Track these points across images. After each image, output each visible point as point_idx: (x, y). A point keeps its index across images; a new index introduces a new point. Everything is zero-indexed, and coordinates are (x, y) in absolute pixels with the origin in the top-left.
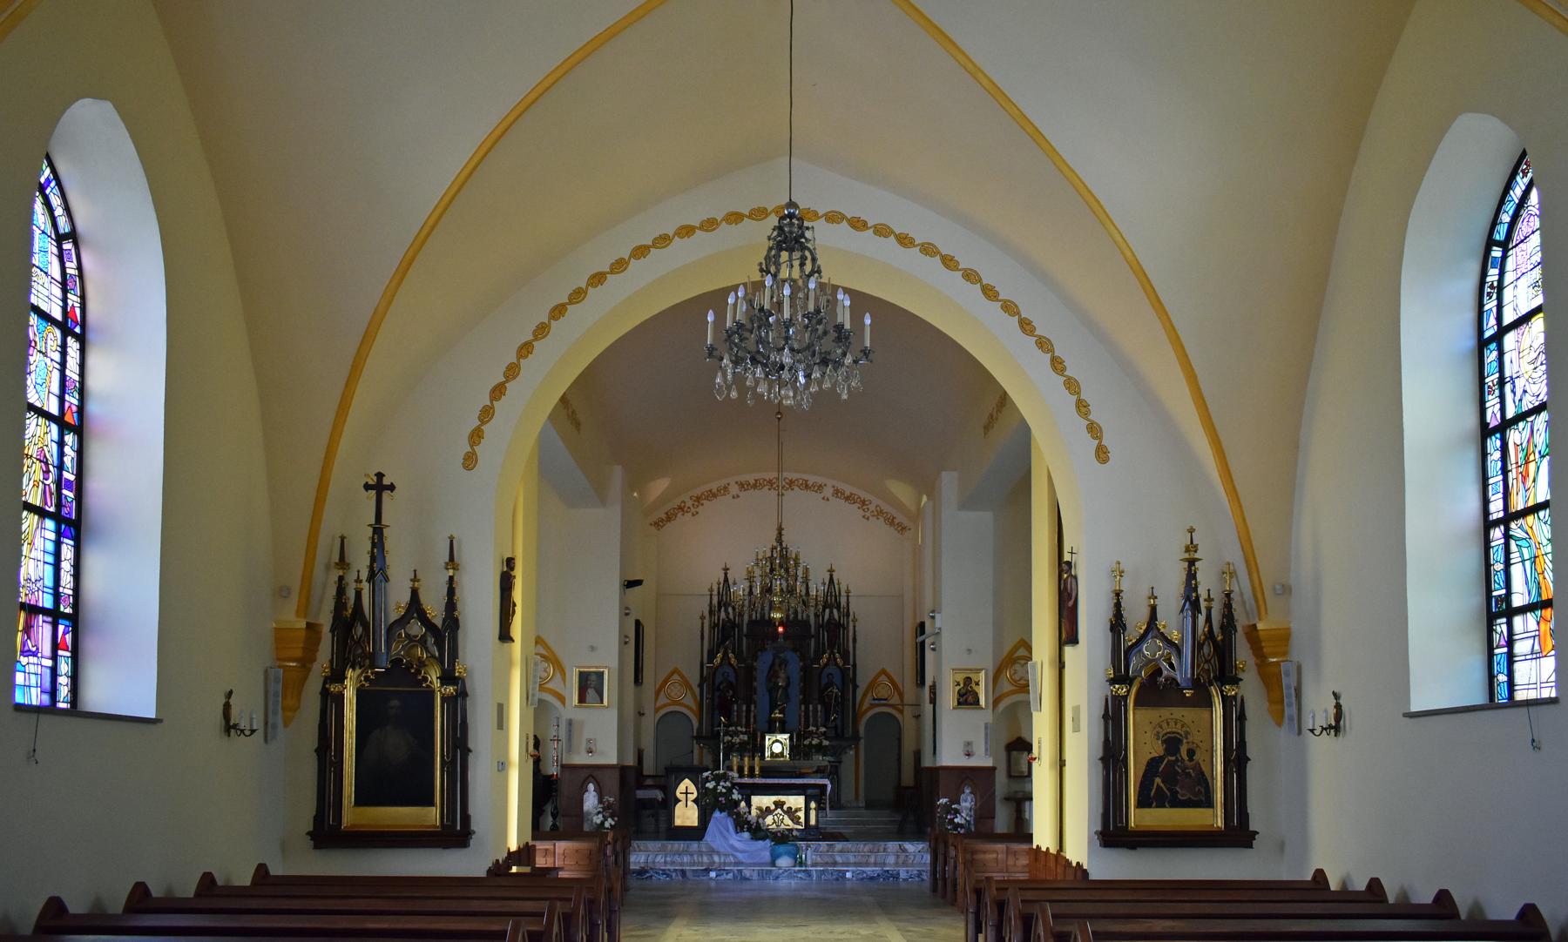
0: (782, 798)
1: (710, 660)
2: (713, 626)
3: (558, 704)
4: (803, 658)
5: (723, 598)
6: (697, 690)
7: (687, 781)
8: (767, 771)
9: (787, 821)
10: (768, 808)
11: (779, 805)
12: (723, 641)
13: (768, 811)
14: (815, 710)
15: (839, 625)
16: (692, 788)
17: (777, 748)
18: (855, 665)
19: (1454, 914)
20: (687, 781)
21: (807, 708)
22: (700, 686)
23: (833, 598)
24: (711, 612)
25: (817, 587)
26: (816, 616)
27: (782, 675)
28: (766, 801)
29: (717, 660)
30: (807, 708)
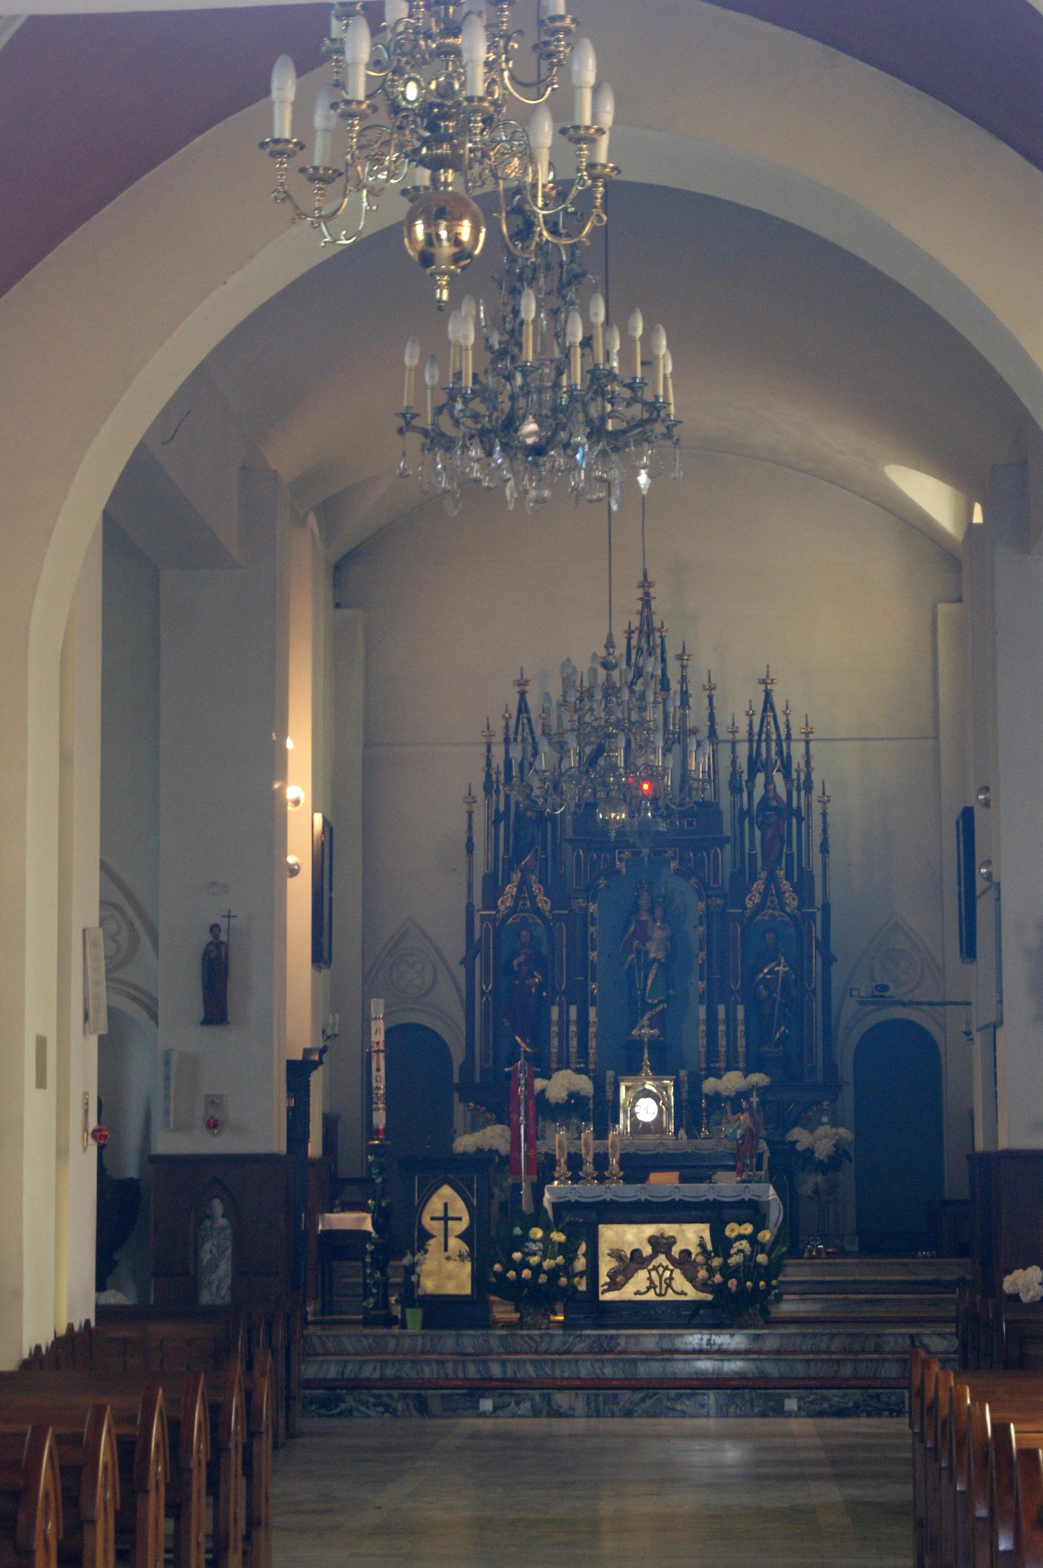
0: (669, 1229)
1: (490, 901)
2: (497, 818)
3: (143, 1016)
4: (704, 891)
5: (566, 743)
6: (460, 972)
7: (446, 1190)
8: (636, 1166)
9: (680, 1282)
10: (636, 1253)
11: (661, 1245)
12: (518, 857)
13: (635, 1261)
14: (583, 1020)
15: (788, 812)
16: (459, 1208)
17: (647, 1110)
18: (826, 908)
19: (940, 1361)
20: (446, 1190)
21: (712, 1014)
22: (468, 962)
23: (770, 748)
24: (489, 786)
25: (737, 710)
26: (735, 788)
27: (658, 934)
28: (633, 1236)
29: (504, 903)
30: (712, 1014)
